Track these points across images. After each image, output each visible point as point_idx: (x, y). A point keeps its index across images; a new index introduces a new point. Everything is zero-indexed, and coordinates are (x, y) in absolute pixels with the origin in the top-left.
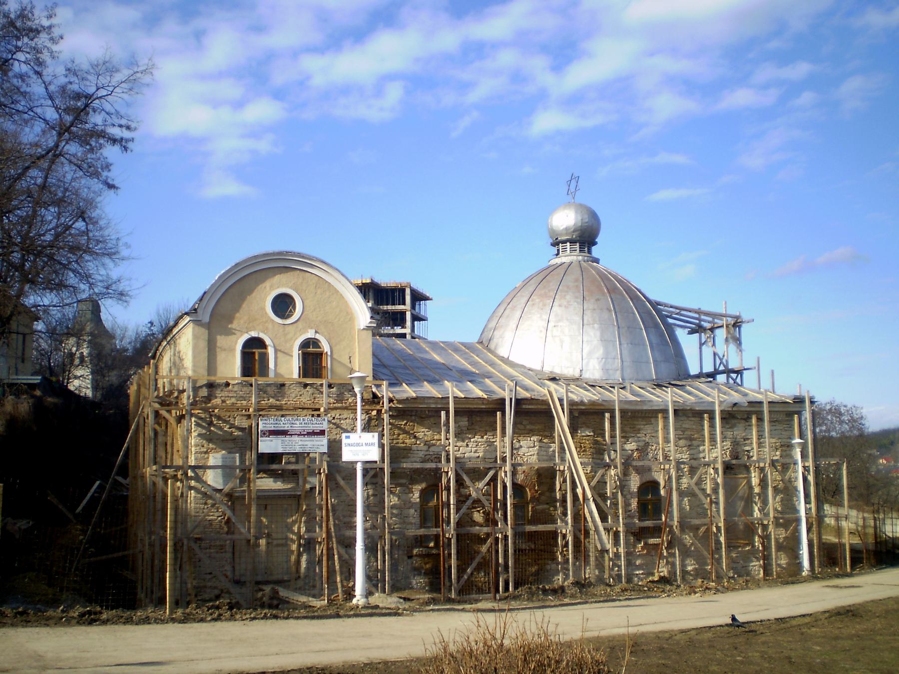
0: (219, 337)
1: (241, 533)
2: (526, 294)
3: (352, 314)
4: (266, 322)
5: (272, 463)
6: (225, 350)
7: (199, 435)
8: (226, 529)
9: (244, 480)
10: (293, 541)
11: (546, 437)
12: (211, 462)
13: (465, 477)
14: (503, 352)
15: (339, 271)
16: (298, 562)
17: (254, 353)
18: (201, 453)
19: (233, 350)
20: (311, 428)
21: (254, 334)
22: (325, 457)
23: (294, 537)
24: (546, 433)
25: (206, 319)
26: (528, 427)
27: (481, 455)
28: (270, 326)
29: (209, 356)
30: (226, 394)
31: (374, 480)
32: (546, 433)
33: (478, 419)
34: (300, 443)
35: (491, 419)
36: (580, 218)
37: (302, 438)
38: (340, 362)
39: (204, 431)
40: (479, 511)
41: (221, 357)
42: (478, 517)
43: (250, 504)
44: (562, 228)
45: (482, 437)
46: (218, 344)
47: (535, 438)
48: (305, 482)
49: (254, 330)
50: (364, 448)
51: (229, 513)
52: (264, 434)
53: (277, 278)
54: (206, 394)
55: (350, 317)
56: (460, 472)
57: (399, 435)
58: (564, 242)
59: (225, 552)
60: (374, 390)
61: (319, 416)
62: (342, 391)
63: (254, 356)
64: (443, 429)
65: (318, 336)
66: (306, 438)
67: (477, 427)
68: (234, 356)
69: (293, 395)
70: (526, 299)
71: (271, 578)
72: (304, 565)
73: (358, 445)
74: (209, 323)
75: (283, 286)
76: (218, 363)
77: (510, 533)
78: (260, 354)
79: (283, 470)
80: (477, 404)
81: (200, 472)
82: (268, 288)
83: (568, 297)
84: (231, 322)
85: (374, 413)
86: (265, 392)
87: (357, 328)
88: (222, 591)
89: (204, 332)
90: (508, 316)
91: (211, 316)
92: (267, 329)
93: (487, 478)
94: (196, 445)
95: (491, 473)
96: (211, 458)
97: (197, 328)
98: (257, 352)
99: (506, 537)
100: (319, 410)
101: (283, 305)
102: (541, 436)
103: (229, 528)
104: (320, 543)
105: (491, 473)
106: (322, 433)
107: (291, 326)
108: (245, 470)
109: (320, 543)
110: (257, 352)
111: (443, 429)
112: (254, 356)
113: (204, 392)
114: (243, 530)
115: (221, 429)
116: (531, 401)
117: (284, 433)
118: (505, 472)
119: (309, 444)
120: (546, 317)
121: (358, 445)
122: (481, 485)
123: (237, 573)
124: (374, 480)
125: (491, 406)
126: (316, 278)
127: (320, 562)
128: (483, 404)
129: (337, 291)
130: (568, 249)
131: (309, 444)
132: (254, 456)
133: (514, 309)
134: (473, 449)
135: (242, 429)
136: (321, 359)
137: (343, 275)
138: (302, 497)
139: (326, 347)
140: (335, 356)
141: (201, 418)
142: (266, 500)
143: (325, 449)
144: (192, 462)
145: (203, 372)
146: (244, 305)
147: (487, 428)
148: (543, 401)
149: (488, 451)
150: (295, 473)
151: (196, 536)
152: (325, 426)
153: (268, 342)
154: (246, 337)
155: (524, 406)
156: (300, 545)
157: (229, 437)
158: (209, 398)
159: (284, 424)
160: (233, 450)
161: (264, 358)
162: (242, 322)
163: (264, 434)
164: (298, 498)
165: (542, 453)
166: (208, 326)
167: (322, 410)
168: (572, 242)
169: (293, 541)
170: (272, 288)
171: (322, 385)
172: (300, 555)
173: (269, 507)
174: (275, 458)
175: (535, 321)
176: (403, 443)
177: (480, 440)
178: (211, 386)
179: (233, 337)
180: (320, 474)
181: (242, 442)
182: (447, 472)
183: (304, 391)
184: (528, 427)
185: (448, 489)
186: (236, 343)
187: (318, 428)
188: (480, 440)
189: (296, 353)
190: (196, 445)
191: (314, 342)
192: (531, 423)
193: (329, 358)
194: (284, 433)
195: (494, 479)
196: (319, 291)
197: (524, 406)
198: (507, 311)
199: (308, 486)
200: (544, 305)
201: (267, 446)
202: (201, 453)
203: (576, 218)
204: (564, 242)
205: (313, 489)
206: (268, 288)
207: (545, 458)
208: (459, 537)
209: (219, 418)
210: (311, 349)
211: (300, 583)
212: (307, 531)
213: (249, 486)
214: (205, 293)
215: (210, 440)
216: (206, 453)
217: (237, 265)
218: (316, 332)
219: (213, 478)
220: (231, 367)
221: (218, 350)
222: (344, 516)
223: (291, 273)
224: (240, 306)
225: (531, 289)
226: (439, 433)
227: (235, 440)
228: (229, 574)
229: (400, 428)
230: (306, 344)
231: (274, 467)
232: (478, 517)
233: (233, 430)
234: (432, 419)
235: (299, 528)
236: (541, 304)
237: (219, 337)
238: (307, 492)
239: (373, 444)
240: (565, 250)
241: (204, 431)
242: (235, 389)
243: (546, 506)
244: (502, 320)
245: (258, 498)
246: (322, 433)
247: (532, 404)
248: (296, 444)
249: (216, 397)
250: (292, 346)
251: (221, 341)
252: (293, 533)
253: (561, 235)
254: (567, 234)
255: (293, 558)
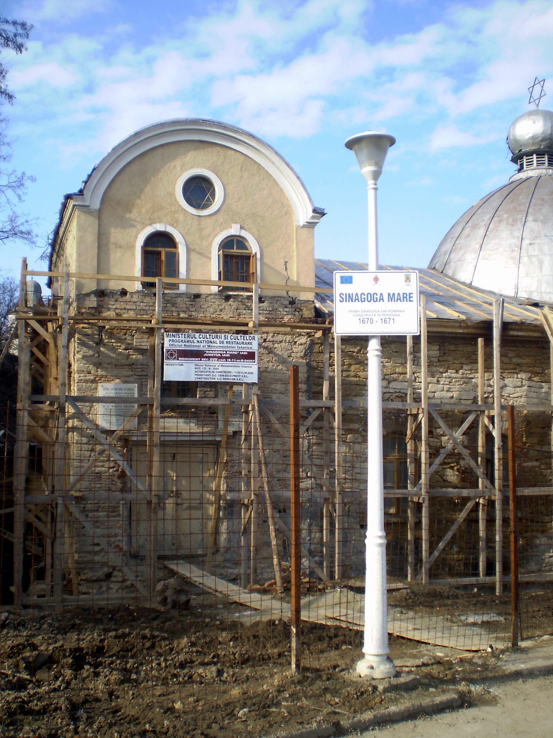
0: (112, 230)
1: (138, 491)
2: (495, 202)
3: (289, 206)
4: (176, 212)
5: (185, 396)
6: (120, 247)
7: (84, 357)
8: (119, 485)
9: (143, 418)
10: (210, 503)
11: (537, 374)
12: (101, 392)
13: (441, 422)
14: (464, 276)
15: (272, 148)
16: (216, 532)
17: (159, 253)
18: (86, 381)
19: (131, 247)
20: (236, 349)
21: (160, 227)
22: (255, 390)
23: (212, 498)
24: (538, 370)
25: (96, 205)
26: (515, 360)
27: (455, 395)
28: (181, 217)
29: (98, 255)
30: (123, 305)
31: (318, 424)
32: (538, 370)
33: (452, 348)
34: (221, 369)
35: (470, 349)
36: (549, 125)
37: (223, 362)
38: (272, 268)
39: (91, 353)
40: (452, 468)
41: (115, 255)
42: (452, 476)
43: (151, 451)
44: (527, 137)
45: (457, 372)
46: (112, 240)
47: (522, 375)
48: (227, 423)
49: (160, 222)
50: (386, 305)
51: (123, 465)
52: (171, 355)
53: (192, 156)
54: (95, 304)
55: (285, 209)
56: (435, 415)
57: (350, 365)
58: (529, 154)
59: (119, 515)
60: (318, 305)
61: (245, 333)
62: (276, 306)
63: (159, 251)
64: (409, 358)
65: (244, 234)
66: (229, 363)
67: (450, 358)
68: (133, 255)
69: (212, 310)
70: (491, 215)
71: (181, 552)
72: (223, 537)
73: (372, 298)
74: (100, 210)
75: (198, 166)
76: (112, 263)
77: (497, 497)
78: (167, 253)
79: (196, 407)
80: (453, 327)
81: (83, 406)
82: (178, 169)
83: (544, 211)
84: (130, 212)
85: (319, 334)
86: (174, 305)
87: (295, 224)
88: (114, 568)
89: (92, 222)
90: (468, 236)
91: (103, 201)
92: (177, 221)
93: (465, 425)
94: (80, 372)
95: (471, 418)
96: (100, 388)
97: (83, 216)
98: (163, 251)
99: (491, 504)
100: (247, 325)
101: (198, 190)
102: (531, 372)
103: (124, 483)
104: (247, 507)
105: (471, 418)
106: (250, 356)
107: (208, 220)
108: (146, 405)
109: (247, 507)
110: (163, 251)
111: (409, 358)
112: (159, 251)
113: (92, 302)
114: (140, 487)
115: (114, 349)
116: (521, 325)
117: (198, 354)
118: (492, 419)
119: (233, 370)
120: (518, 234)
121: (372, 298)
122: (458, 434)
123: (134, 544)
124: (318, 424)
125: (470, 331)
126: (242, 157)
127: (246, 531)
128: (460, 327)
129: (269, 176)
130: (535, 162)
131: (233, 370)
132: (157, 385)
133: (474, 227)
134: (446, 387)
135: (142, 351)
136: (248, 264)
137: (288, 165)
138: (223, 444)
139: (254, 247)
140: (266, 261)
141: (86, 335)
142: (173, 447)
143: (254, 379)
144: (75, 392)
145: (91, 267)
146: (147, 189)
147: (463, 360)
148: (536, 326)
149: (464, 390)
150: (212, 411)
151: (77, 494)
152: (254, 347)
153: (178, 238)
154: (148, 231)
155: (512, 333)
156: (218, 509)
157: (124, 361)
158: (98, 309)
159: (198, 342)
160: (131, 379)
161: (173, 259)
162: (144, 211)
163: (171, 355)
164: (217, 445)
165: (532, 394)
166: (99, 214)
167: (251, 324)
168: (540, 154)
169: (210, 503)
170: (183, 168)
171: (250, 298)
172: (218, 521)
173: (178, 457)
174: (185, 388)
175: (505, 238)
176: (356, 376)
177: (454, 375)
178: (101, 294)
179: (132, 231)
180: (247, 412)
181: (142, 366)
182: (416, 416)
183: (225, 305)
184: (515, 360)
185: (416, 437)
186: (136, 237)
187: (245, 349)
188: (454, 375)
189: (215, 253)
190: (80, 372)
191: (240, 242)
192: (518, 356)
193: (259, 263)
194: (198, 354)
195: (474, 426)
196: (246, 174)
197: (512, 333)
198: (467, 231)
199: (231, 430)
200: (515, 221)
201: (176, 371)
202: (86, 381)
203: (545, 125)
204: (529, 154)
205: (236, 433)
206: (178, 169)
207: (535, 401)
208: (433, 500)
209: (111, 335)
210: (235, 251)
211: (219, 558)
212: (230, 490)
213: (151, 427)
214: (94, 169)
215: (98, 365)
216: (93, 381)
217: (137, 134)
218: (242, 228)
219: (103, 417)
220: (128, 268)
221: (112, 247)
222: (278, 472)
223: (210, 150)
224: (142, 191)
225: (496, 204)
226: (404, 364)
227: (132, 365)
228: (125, 548)
229: (351, 357)
230: (228, 243)
231: (186, 401)
232: (452, 476)
233: (131, 352)
234: (393, 346)
235: (218, 486)
236: (510, 221)
237: (112, 230)
238: (229, 437)
239: (407, 297)
240: (530, 164)
241: (91, 353)
242: (135, 299)
243: (536, 464)
244: (461, 241)
245: (163, 444)
246: (250, 356)
247: (521, 330)
248: (216, 371)
249: (109, 309)
250: (210, 246)
251: (116, 235)
252: (210, 491)
253: (526, 145)
254: (533, 144)
255: (211, 524)
